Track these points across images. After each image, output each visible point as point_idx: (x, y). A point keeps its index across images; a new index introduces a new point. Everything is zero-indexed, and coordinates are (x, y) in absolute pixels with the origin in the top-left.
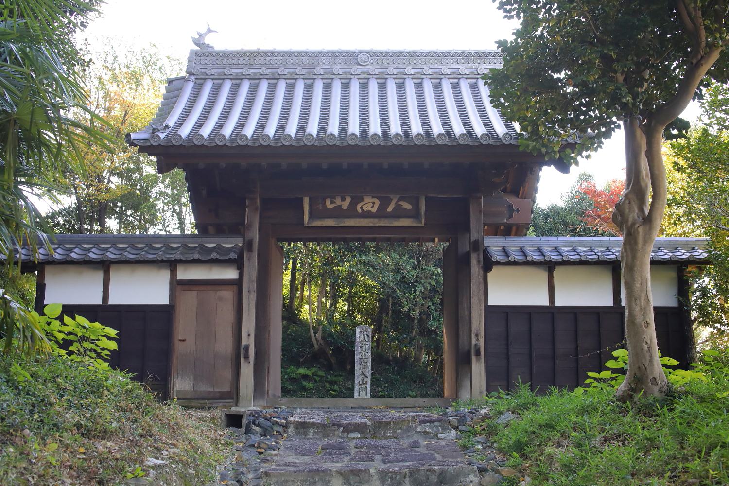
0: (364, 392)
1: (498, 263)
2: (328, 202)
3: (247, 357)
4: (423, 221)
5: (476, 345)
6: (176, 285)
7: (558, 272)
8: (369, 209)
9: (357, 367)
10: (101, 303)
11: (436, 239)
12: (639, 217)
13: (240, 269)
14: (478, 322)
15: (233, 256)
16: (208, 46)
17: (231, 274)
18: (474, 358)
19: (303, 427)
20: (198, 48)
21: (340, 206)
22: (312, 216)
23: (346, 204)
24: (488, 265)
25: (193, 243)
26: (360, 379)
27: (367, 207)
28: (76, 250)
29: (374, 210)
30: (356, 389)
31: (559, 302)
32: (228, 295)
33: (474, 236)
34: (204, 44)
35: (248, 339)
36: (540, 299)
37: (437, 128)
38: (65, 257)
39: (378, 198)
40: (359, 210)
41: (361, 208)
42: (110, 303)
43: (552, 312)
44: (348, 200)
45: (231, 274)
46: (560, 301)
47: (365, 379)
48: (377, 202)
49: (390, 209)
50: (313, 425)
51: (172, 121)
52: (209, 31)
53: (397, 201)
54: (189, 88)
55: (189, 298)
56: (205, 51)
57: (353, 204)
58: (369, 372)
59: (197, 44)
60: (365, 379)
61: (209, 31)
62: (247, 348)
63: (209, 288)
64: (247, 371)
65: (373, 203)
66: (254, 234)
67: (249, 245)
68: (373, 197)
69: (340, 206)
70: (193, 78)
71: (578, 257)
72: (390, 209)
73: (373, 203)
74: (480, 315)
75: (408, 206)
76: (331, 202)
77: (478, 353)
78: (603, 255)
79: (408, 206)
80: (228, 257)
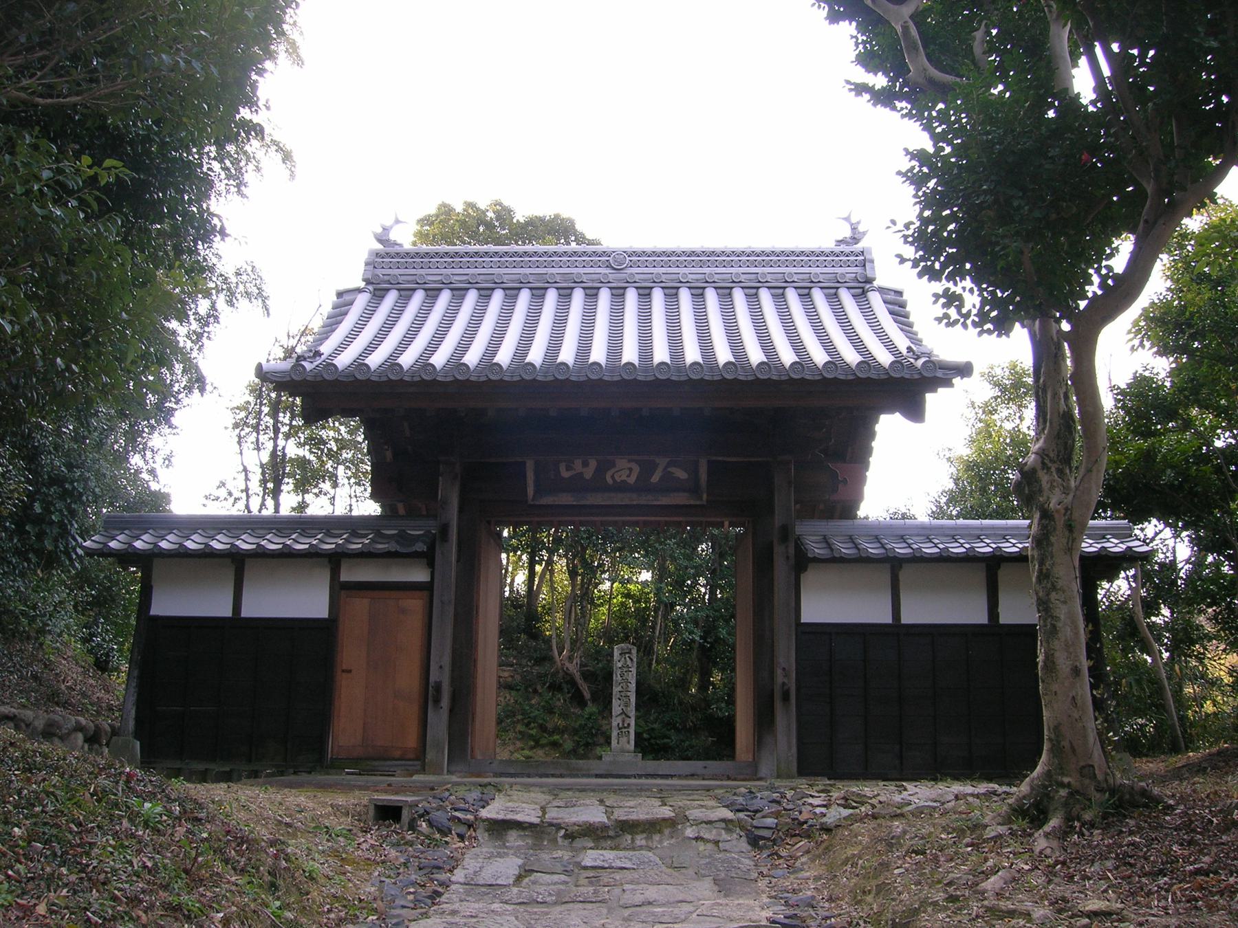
0: (625, 739)
1: (817, 560)
2: (562, 467)
3: (437, 701)
4: (705, 496)
5: (784, 684)
6: (339, 590)
7: (905, 575)
8: (624, 478)
9: (615, 702)
10: (230, 615)
11: (726, 523)
12: (102, 665)
13: (431, 564)
14: (786, 656)
15: (420, 547)
16: (395, 244)
17: (419, 575)
18: (778, 704)
19: (499, 828)
20: (380, 247)
21: (582, 473)
22: (538, 492)
23: (589, 473)
24: (802, 562)
25: (388, 528)
26: (619, 720)
27: (622, 476)
28: (143, 537)
29: (632, 480)
30: (614, 734)
31: (906, 619)
32: (415, 604)
33: (778, 520)
34: (388, 240)
35: (441, 673)
36: (882, 616)
37: (724, 355)
38: (101, 546)
39: (636, 462)
40: (609, 481)
41: (612, 477)
42: (243, 615)
43: (896, 633)
44: (593, 464)
45: (419, 575)
46: (909, 616)
47: (627, 721)
48: (636, 469)
49: (655, 478)
50: (518, 825)
51: (326, 348)
52: (397, 222)
53: (666, 467)
54: (362, 301)
55: (359, 606)
56: (389, 250)
57: (600, 471)
58: (632, 712)
59: (380, 241)
60: (627, 721)
61: (397, 222)
62: (438, 687)
63: (387, 593)
64: (439, 723)
65: (631, 470)
66: (452, 515)
67: (444, 530)
68: (630, 461)
69: (582, 473)
70: (371, 288)
71: (909, 551)
72: (655, 478)
73: (631, 470)
74: (790, 748)
75: (681, 474)
76: (568, 468)
77: (786, 697)
78: (947, 548)
79: (681, 474)
80: (413, 549)
